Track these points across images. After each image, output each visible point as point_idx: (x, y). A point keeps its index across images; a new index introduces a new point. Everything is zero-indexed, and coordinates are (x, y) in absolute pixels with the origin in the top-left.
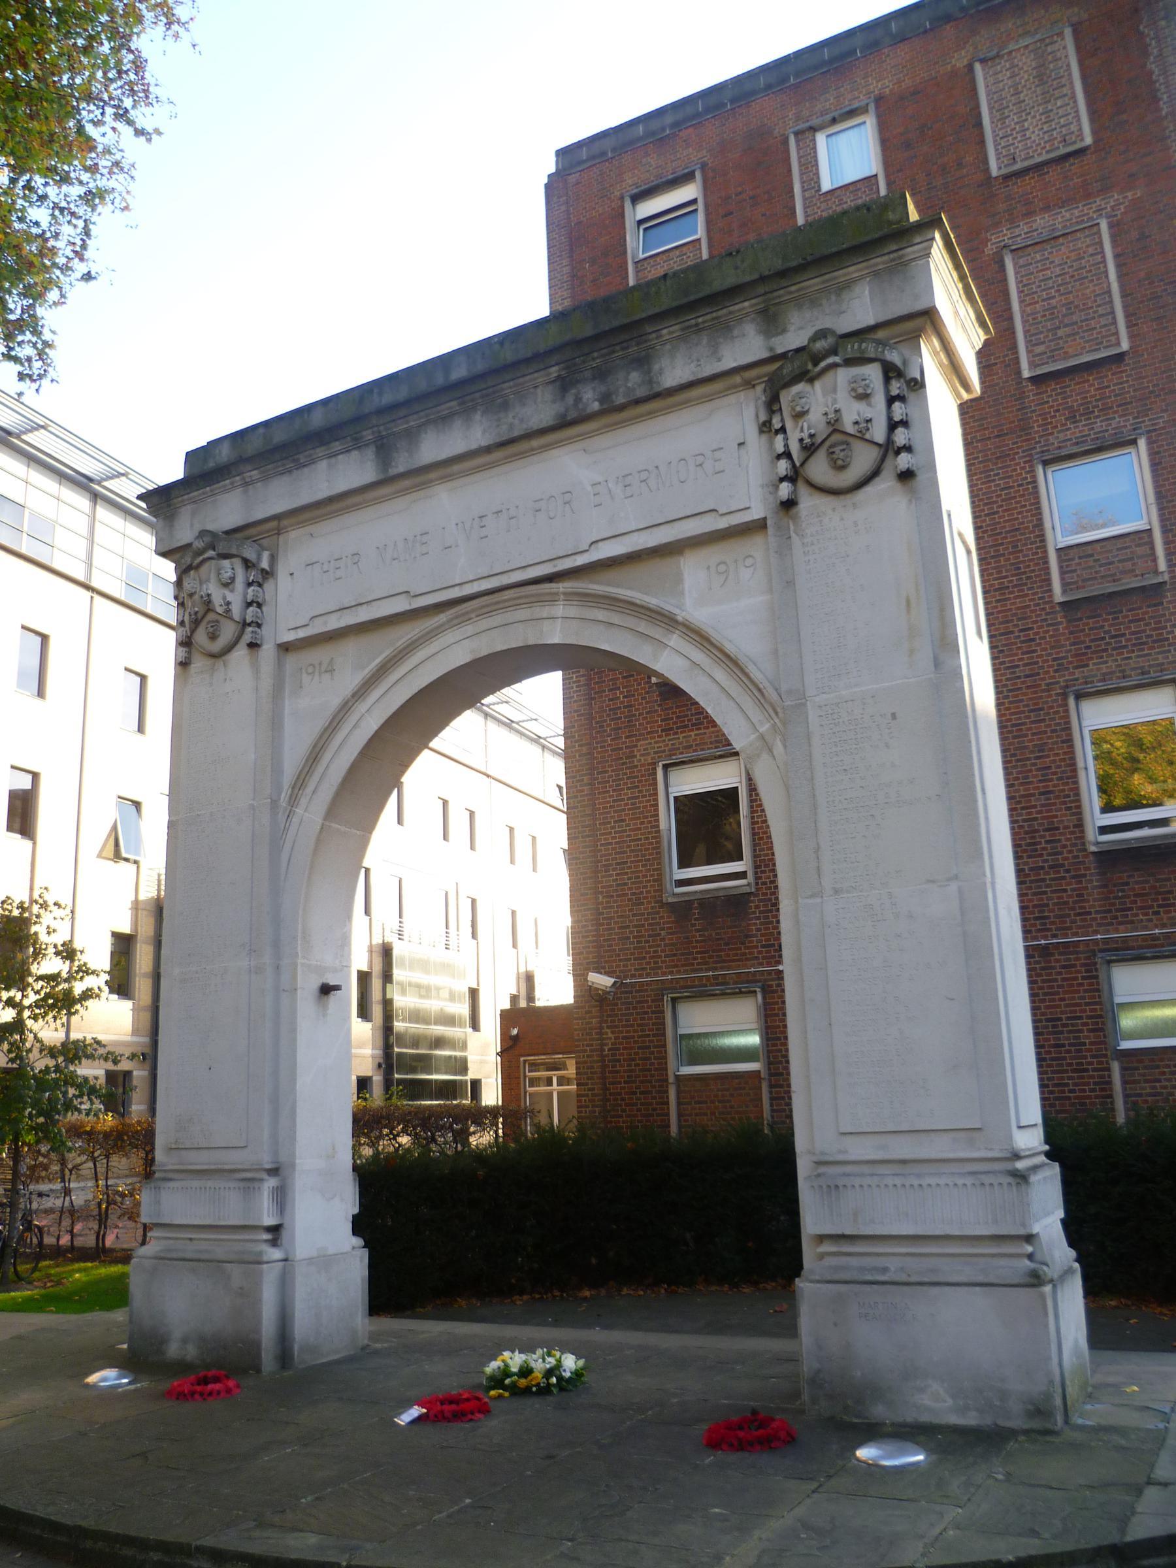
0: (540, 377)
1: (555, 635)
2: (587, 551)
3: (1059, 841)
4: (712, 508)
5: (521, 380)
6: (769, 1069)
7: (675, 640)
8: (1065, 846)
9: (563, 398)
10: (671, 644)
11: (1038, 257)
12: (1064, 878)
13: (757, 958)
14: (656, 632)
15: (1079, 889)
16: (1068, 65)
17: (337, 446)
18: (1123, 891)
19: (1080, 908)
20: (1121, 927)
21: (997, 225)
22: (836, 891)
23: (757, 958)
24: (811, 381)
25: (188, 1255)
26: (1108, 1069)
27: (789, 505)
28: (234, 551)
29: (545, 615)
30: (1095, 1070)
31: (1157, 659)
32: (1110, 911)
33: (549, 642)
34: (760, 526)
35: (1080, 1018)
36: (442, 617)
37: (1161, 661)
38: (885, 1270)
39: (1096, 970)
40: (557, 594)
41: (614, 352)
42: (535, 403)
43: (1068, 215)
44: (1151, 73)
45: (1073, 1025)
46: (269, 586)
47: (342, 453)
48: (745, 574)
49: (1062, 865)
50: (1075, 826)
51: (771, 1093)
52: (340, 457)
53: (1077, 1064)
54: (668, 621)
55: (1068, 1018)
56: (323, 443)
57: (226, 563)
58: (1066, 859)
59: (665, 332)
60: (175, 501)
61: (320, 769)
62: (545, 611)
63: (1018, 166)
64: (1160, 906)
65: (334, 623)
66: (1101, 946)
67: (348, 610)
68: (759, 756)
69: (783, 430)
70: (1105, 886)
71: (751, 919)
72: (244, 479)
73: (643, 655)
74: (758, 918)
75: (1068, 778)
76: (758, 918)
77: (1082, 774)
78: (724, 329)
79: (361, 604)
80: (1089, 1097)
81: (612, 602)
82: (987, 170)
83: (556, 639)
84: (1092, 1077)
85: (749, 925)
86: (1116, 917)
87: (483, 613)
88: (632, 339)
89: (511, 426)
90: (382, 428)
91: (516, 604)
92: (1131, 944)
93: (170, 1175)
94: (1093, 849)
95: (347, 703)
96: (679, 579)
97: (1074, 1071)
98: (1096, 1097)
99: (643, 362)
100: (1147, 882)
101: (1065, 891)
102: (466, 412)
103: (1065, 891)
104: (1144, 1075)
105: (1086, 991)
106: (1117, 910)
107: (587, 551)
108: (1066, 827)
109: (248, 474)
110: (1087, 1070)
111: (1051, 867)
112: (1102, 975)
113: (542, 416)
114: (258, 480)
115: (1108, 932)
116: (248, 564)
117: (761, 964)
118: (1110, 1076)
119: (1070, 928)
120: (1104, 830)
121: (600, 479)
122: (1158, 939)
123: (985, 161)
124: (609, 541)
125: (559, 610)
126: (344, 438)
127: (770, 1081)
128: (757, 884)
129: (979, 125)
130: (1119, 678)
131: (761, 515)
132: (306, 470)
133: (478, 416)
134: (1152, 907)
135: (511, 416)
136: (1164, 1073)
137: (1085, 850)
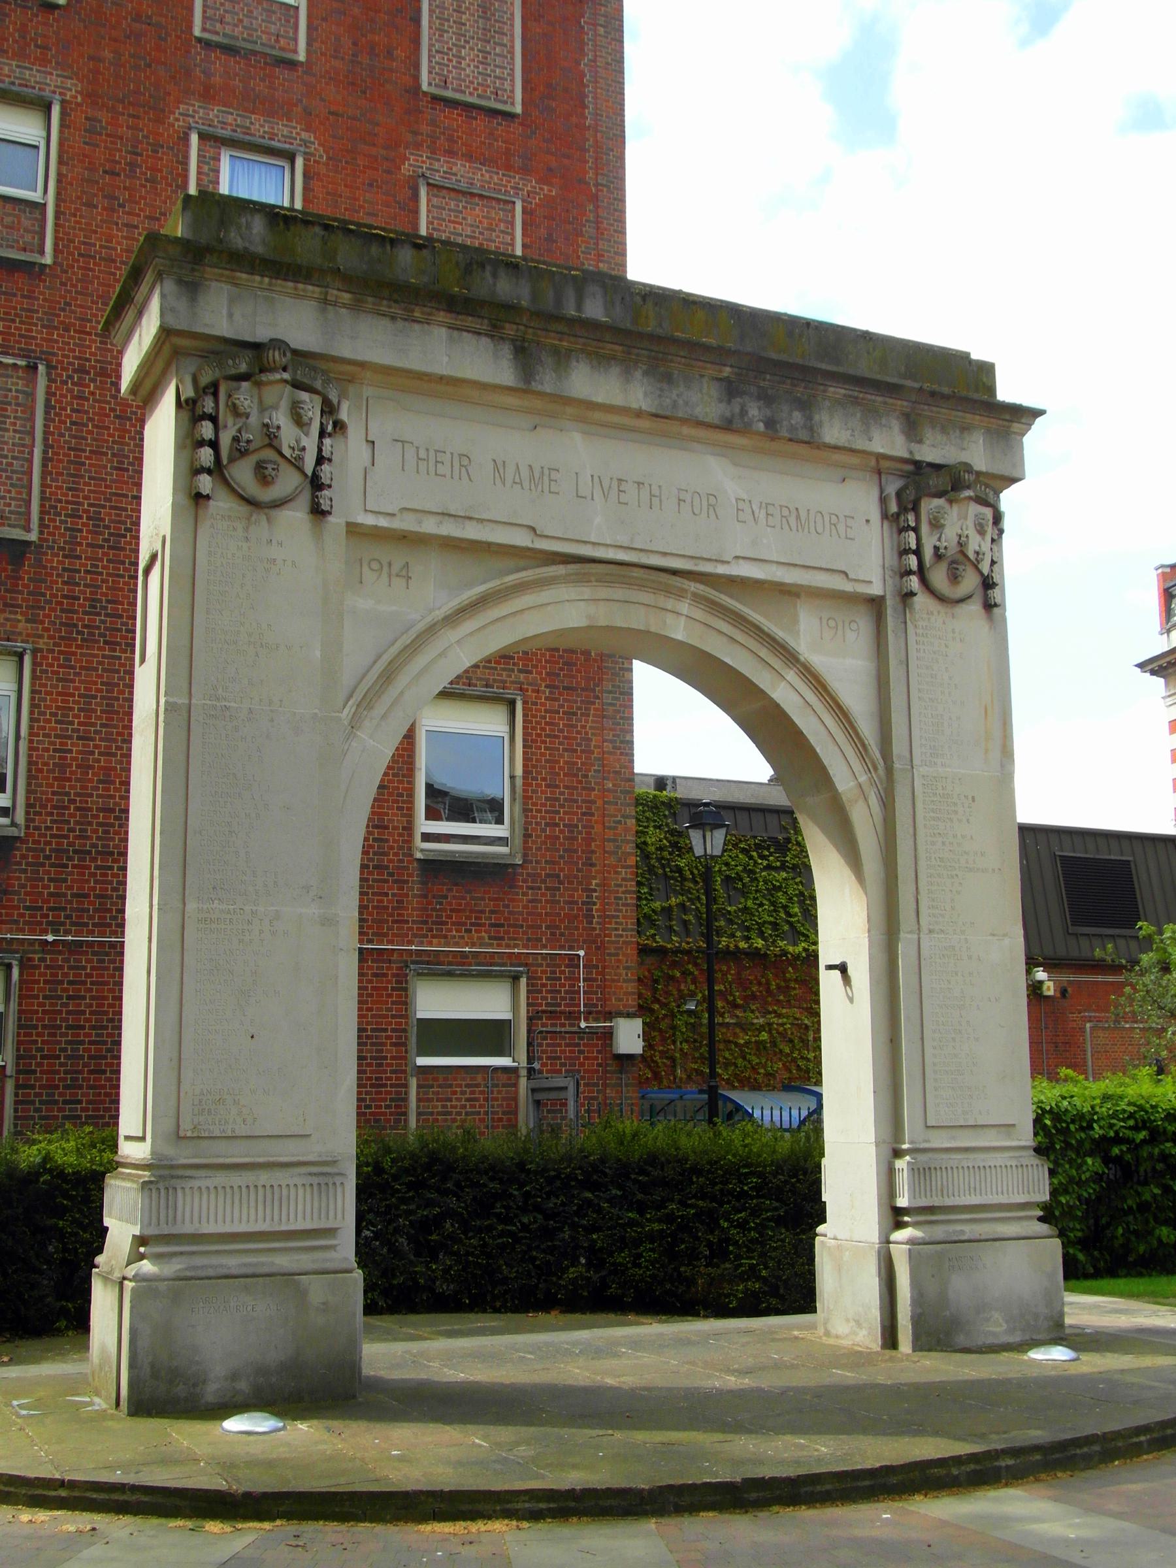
0: (711, 371)
1: (679, 632)
2: (729, 562)
3: (387, 841)
4: (843, 569)
5: (693, 363)
6: (18, 1064)
7: (791, 675)
8: (392, 848)
9: (729, 402)
10: (788, 678)
11: (452, 205)
12: (386, 881)
13: (16, 922)
14: (776, 663)
15: (400, 895)
16: (512, 14)
17: (469, 321)
18: (441, 904)
19: (399, 915)
20: (435, 941)
21: (418, 146)
22: (931, 931)
23: (16, 922)
24: (951, 502)
25: (234, 1271)
26: (406, 1086)
27: (907, 596)
28: (318, 385)
29: (669, 607)
30: (392, 1086)
31: (501, 675)
32: (426, 923)
33: (673, 636)
34: (875, 604)
35: (385, 1030)
36: (560, 570)
37: (504, 678)
38: (962, 1232)
39: (407, 982)
40: (686, 591)
41: (784, 383)
42: (701, 391)
43: (487, 176)
44: (583, 75)
45: (377, 1037)
46: (339, 440)
47: (469, 331)
48: (851, 636)
49: (387, 867)
50: (404, 828)
51: (16, 1095)
52: (465, 334)
53: (377, 1079)
54: (790, 657)
55: (373, 1030)
56: (450, 309)
57: (304, 396)
58: (390, 861)
59: (832, 389)
60: (208, 269)
61: (393, 692)
62: (670, 604)
63: (449, 94)
64: (472, 924)
65: (429, 526)
66: (414, 958)
67: (452, 519)
68: (856, 801)
69: (916, 530)
70: (425, 896)
71: (15, 871)
72: (327, 293)
73: (762, 679)
74: (25, 871)
75: (404, 776)
76: (25, 871)
77: (417, 773)
78: (871, 415)
79: (470, 518)
80: (384, 1114)
81: (739, 620)
82: (417, 78)
83: (679, 636)
84: (390, 1093)
85: (9, 878)
86: (431, 930)
87: (602, 580)
88: (803, 380)
89: (675, 404)
90: (530, 331)
91: (641, 586)
92: (497, 960)
93: (180, 1172)
94: (419, 855)
95: (435, 624)
96: (795, 621)
97: (372, 1086)
98: (391, 1113)
99: (806, 406)
100: (464, 898)
101: (387, 895)
102: (627, 364)
103: (387, 895)
104: (438, 1093)
105: (393, 1003)
106: (434, 923)
107: (729, 562)
108: (395, 828)
109: (335, 292)
110: (385, 1085)
111: (375, 867)
112: (410, 986)
113: (708, 410)
114: (344, 306)
115: (421, 944)
116: (328, 408)
117: (22, 931)
118: (406, 1093)
119: (386, 935)
120: (427, 837)
121: (745, 497)
122: (467, 957)
123: (417, 66)
124: (753, 563)
125: (684, 607)
126: (483, 317)
127: (17, 1080)
128: (27, 827)
129: (417, 21)
130: (464, 684)
131: (880, 593)
132: (416, 326)
133: (638, 374)
134: (465, 924)
135: (675, 392)
136: (455, 1093)
137: (412, 855)
